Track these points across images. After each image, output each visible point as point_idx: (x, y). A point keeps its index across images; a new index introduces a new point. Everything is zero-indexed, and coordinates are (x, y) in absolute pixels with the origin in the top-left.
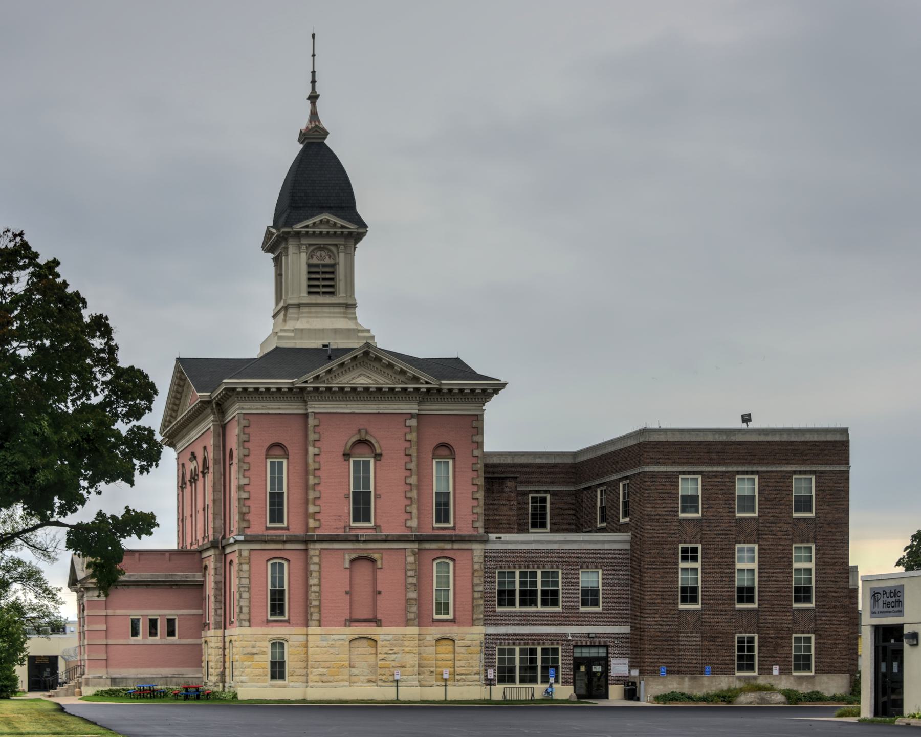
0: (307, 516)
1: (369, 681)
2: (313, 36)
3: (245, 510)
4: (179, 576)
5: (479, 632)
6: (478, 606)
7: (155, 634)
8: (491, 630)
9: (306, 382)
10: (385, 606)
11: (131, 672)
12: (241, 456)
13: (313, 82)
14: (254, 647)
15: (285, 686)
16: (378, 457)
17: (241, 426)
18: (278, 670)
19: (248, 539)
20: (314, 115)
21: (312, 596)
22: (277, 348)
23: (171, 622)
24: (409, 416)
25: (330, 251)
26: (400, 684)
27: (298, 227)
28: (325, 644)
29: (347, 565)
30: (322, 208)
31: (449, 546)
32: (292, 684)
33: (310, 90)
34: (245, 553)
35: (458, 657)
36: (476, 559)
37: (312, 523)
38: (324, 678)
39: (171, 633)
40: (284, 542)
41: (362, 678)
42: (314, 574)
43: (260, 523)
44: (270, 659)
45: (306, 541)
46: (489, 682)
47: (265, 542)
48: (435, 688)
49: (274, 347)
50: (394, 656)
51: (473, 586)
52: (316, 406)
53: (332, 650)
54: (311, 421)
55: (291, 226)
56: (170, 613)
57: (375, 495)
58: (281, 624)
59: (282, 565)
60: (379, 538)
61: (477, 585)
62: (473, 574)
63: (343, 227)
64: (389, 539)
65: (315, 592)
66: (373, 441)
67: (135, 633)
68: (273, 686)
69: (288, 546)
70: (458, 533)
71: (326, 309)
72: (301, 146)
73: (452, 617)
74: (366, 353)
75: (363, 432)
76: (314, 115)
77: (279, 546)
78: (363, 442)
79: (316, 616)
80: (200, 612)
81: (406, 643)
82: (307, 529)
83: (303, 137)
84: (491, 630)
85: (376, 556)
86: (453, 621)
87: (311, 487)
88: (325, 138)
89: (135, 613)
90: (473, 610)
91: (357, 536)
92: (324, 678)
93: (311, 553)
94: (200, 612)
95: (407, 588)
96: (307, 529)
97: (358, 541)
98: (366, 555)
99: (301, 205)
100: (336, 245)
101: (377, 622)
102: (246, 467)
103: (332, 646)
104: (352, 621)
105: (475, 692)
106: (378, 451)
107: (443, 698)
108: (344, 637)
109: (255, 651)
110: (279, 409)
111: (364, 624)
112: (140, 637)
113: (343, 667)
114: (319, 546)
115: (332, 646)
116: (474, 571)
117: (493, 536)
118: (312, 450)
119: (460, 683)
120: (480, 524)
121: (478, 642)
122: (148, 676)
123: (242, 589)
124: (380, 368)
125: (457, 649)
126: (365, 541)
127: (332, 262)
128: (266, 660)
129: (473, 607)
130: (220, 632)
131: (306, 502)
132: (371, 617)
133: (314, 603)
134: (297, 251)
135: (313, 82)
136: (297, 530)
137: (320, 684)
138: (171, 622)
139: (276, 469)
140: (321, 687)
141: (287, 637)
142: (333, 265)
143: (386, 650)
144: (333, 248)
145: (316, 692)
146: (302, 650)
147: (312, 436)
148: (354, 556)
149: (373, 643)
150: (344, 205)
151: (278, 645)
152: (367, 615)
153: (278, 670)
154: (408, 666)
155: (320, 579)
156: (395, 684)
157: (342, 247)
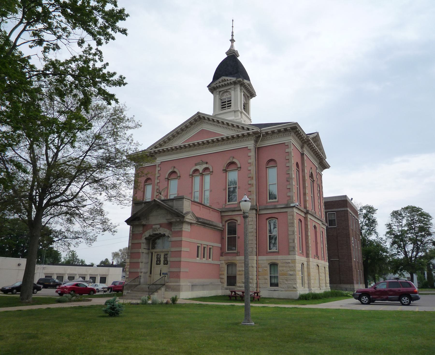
2: (233, 20)
13: (232, 35)
20: (232, 46)
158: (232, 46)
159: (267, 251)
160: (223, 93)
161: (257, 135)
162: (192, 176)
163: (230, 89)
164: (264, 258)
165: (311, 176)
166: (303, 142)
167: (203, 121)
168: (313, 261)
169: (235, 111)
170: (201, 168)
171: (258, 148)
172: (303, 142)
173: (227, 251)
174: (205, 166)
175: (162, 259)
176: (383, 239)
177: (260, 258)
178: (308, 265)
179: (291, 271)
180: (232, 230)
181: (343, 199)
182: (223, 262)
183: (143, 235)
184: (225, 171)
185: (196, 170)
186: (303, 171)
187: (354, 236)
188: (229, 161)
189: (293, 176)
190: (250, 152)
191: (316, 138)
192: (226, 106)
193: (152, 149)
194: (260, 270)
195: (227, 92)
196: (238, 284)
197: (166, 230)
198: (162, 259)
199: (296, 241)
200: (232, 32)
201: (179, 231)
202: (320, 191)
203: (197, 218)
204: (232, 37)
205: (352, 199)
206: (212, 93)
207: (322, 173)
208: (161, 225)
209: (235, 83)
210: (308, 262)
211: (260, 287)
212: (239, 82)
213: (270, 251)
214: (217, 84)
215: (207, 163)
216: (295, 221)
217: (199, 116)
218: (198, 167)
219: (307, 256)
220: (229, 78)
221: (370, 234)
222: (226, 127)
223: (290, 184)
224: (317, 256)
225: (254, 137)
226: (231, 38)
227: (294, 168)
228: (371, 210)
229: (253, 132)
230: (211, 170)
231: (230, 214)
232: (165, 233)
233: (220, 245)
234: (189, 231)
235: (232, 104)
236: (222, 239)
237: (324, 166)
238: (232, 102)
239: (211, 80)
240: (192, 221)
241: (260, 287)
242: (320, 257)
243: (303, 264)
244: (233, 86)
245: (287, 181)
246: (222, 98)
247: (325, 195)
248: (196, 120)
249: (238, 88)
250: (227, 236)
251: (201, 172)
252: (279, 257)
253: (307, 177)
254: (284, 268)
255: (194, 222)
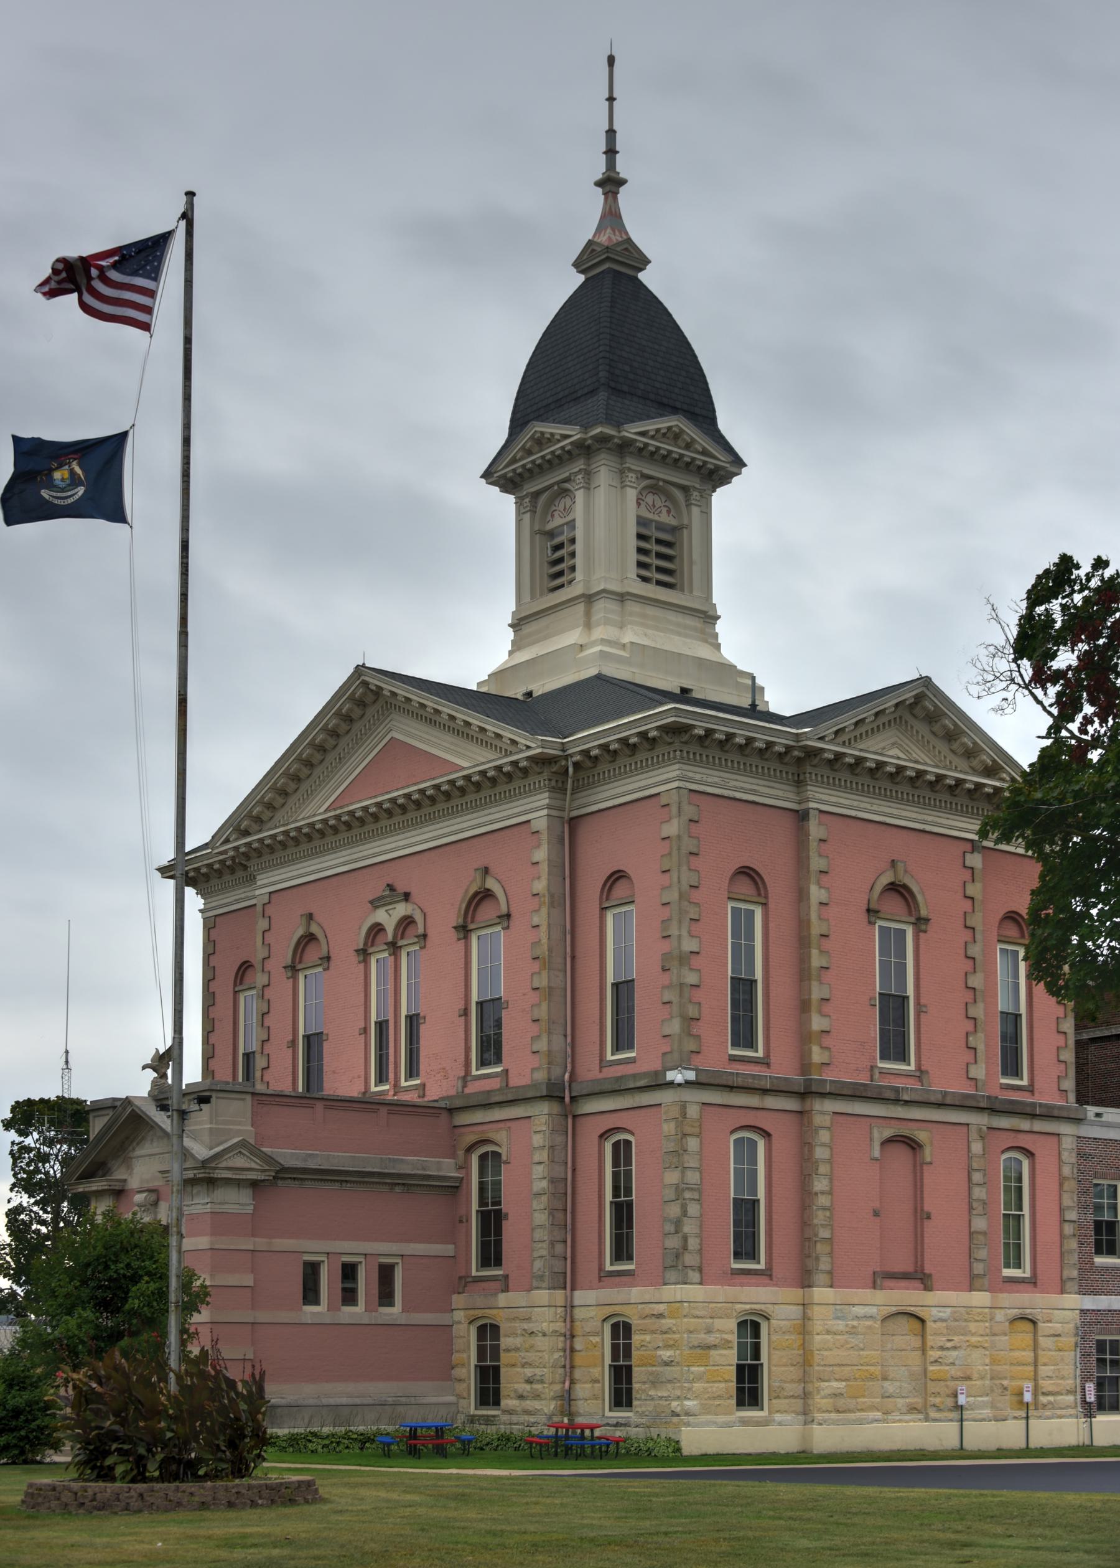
0: (805, 1038)
1: (912, 1409)
2: (611, 60)
3: (692, 1011)
4: (410, 1163)
5: (1071, 1304)
6: (1070, 1252)
7: (316, 1302)
8: (1090, 1302)
9: (822, 739)
10: (943, 1241)
11: (340, 1392)
12: (685, 886)
13: (611, 152)
14: (709, 1331)
15: (765, 1423)
16: (920, 923)
17: (685, 818)
18: (748, 1388)
19: (703, 1079)
20: (612, 216)
21: (820, 1218)
22: (599, 677)
23: (386, 1273)
24: (968, 846)
25: (669, 497)
26: (967, 1414)
27: (631, 431)
28: (840, 1325)
29: (877, 1153)
30: (675, 410)
31: (1025, 1125)
32: (778, 1417)
33: (602, 168)
34: (693, 1111)
35: (1043, 1356)
36: (1065, 1156)
37: (817, 1055)
38: (841, 1403)
39: (386, 1296)
40: (765, 1092)
41: (901, 1402)
42: (823, 1169)
43: (720, 1050)
44: (735, 1361)
45: (806, 1093)
46: (1089, 1410)
47: (731, 1088)
48: (1010, 1423)
49: (592, 672)
50: (954, 1353)
51: (1062, 1210)
52: (822, 798)
53: (853, 1341)
54: (815, 829)
55: (618, 425)
56: (385, 1249)
57: (918, 1003)
58: (753, 1279)
59: (753, 1144)
60: (933, 1099)
61: (1069, 1208)
62: (1061, 1185)
63: (705, 452)
64: (948, 1101)
65: (824, 1209)
66: (915, 889)
67: (311, 1294)
68: (744, 1422)
69: (771, 1102)
70: (1037, 1099)
71: (672, 616)
72: (581, 278)
73: (1028, 1274)
74: (919, 698)
75: (900, 867)
76: (612, 216)
77: (753, 1100)
78: (897, 889)
79: (824, 1264)
80: (448, 1249)
81: (972, 1326)
82: (805, 1067)
83: (589, 260)
84: (1090, 1302)
85: (922, 1136)
86: (1032, 1282)
87: (814, 972)
88: (641, 270)
89: (313, 1248)
90: (1062, 1260)
91: (896, 1090)
92: (841, 1403)
93: (818, 1120)
94: (448, 1249)
95: (971, 1208)
96: (805, 1067)
97: (897, 1101)
98: (906, 1133)
99: (625, 388)
100: (685, 489)
101: (922, 1279)
102: (693, 913)
103: (853, 1331)
104: (883, 1278)
105: (1060, 1429)
106: (924, 913)
107: (955, 1444)
108: (873, 1310)
109: (711, 1339)
110: (754, 792)
111: (904, 1283)
112: (360, 1308)
113: (872, 1378)
114: (830, 1106)
115: (853, 1331)
116: (1062, 1180)
117: (1091, 1110)
118: (816, 894)
119: (1048, 1413)
120: (1069, 1084)
121: (1072, 1325)
122: (344, 1401)
123: (687, 1195)
124: (928, 736)
125: (1042, 1341)
126: (907, 1103)
127: (673, 522)
128: (728, 1359)
129: (1062, 1254)
130: (559, 1296)
131: (804, 1006)
132: (910, 1268)
133: (824, 1233)
134: (616, 483)
135: (611, 152)
136: (784, 1069)
137: (834, 1416)
138: (386, 1273)
139: (742, 925)
140: (835, 1423)
141: (769, 1309)
142: (674, 530)
143: (941, 1340)
144: (678, 495)
145: (830, 1436)
146: (794, 1339)
147: (817, 863)
148: (888, 1133)
149: (917, 1325)
150: (697, 411)
151: (751, 1327)
152: (904, 1264)
153: (748, 1388)
154: (975, 1376)
155: (970, 1179)
156: (955, 1415)
157: (695, 494)
159: (601, 1268)
160: (551, 502)
162: (364, 954)
163: (567, 480)
169: (589, 599)
170: (388, 917)
171: (572, 819)
174: (401, 909)
179: (668, 1347)
185: (377, 929)
193: (227, 841)
196: (506, 1403)
200: (611, 133)
204: (611, 164)
209: (585, 450)
212: (603, 439)
215: (407, 897)
218: (380, 916)
220: (558, 430)
225: (545, 775)
226: (599, 169)
229: (528, 758)
234: (249, 1209)
239: (506, 436)
244: (580, 464)
246: (550, 526)
249: (604, 473)
252: (636, 1293)
254: (648, 1338)
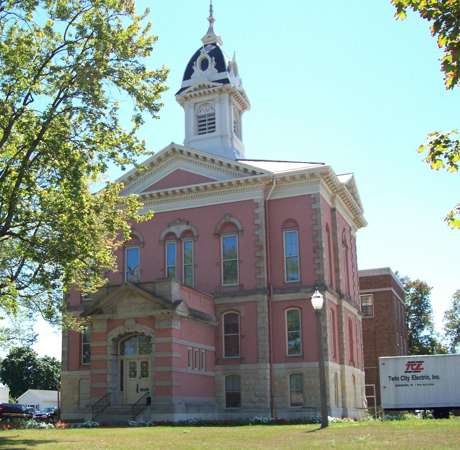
13: (211, 11)
20: (211, 30)
158: (211, 30)
161: (267, 182)
164: (282, 366)
165: (344, 243)
166: (335, 191)
167: (179, 156)
168: (349, 369)
172: (335, 191)
173: (224, 357)
174: (184, 227)
175: (139, 370)
176: (440, 334)
177: (276, 366)
178: (342, 375)
180: (232, 326)
181: (384, 273)
182: (219, 373)
183: (110, 334)
184: (217, 235)
185: (171, 235)
186: (335, 235)
187: (400, 332)
188: (224, 221)
189: (324, 245)
190: (257, 208)
191: (351, 185)
192: (207, 127)
194: (276, 383)
195: (206, 104)
197: (144, 326)
198: (139, 370)
199: (328, 341)
200: (211, 6)
201: (167, 329)
202: (355, 265)
203: (190, 310)
205: (397, 272)
206: (182, 105)
207: (357, 234)
208: (137, 320)
210: (342, 371)
211: (276, 408)
213: (289, 355)
214: (190, 91)
216: (327, 311)
217: (174, 150)
218: (173, 229)
219: (341, 362)
221: (421, 327)
222: (218, 167)
223: (318, 257)
224: (352, 362)
227: (324, 235)
228: (422, 289)
230: (195, 234)
231: (228, 300)
232: (144, 331)
233: (213, 348)
234: (179, 328)
235: (217, 125)
236: (217, 338)
237: (360, 223)
238: (217, 121)
240: (184, 314)
241: (276, 408)
242: (356, 364)
243: (336, 374)
245: (314, 252)
247: (360, 268)
248: (167, 155)
250: (223, 335)
251: (178, 237)
252: (304, 364)
253: (340, 245)
255: (185, 315)
